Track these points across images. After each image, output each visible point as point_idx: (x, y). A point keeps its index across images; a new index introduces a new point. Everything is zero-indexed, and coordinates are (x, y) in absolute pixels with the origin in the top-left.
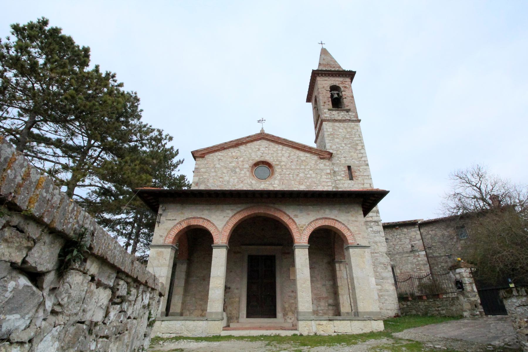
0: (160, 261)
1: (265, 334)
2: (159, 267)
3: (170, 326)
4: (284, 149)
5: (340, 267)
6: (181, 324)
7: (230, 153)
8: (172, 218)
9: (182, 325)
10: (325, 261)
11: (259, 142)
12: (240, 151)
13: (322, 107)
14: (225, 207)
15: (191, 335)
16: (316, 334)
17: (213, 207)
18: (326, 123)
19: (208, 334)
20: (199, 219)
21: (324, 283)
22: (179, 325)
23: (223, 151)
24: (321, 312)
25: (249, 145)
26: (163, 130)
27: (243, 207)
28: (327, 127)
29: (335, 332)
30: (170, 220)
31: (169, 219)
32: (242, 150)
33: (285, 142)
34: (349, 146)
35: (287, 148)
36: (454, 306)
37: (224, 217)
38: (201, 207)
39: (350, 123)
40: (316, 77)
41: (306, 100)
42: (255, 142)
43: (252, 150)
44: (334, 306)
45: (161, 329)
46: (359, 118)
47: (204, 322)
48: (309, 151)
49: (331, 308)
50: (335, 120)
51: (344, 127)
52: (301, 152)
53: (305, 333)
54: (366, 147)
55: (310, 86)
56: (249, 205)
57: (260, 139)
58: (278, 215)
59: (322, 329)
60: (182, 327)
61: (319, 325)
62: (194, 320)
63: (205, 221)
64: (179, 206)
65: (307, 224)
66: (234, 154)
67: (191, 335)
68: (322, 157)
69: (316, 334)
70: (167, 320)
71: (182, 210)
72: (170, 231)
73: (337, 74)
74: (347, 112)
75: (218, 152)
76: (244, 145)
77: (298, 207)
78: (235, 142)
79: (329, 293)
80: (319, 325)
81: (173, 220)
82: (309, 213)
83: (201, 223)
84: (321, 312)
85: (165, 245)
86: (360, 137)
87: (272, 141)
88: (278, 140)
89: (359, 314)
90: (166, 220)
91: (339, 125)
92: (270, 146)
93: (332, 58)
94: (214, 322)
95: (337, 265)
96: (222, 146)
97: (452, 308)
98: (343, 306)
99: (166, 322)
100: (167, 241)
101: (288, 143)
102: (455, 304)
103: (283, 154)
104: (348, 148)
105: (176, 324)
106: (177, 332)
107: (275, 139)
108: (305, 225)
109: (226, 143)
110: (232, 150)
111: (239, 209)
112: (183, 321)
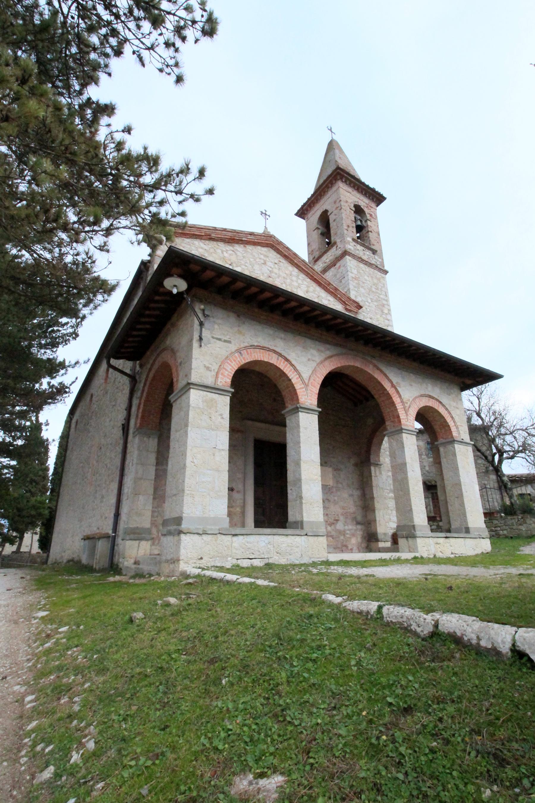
0: (213, 418)
1: (383, 558)
2: (213, 430)
3: (249, 545)
4: (300, 277)
5: (375, 472)
6: (267, 542)
7: (219, 251)
8: (224, 338)
9: (269, 543)
10: (353, 461)
11: (265, 249)
12: (236, 254)
13: (345, 232)
14: (309, 342)
15: (284, 560)
16: (435, 556)
17: (290, 336)
18: (350, 258)
19: (310, 558)
20: (271, 353)
21: (351, 492)
22: (264, 544)
23: (207, 242)
24: (348, 532)
25: (250, 248)
26: (145, 149)
27: (338, 350)
28: (352, 266)
29: (452, 553)
30: (220, 339)
31: (219, 337)
32: (238, 253)
33: (304, 266)
34: (376, 303)
35: (304, 276)
36: (525, 525)
37: (309, 360)
38: (271, 332)
39: (376, 272)
40: (336, 180)
41: (296, 211)
42: (259, 247)
43: (255, 260)
44: (362, 524)
45: (234, 551)
46: (386, 268)
47: (303, 537)
48: (332, 293)
49: (359, 527)
50: (360, 258)
51: (370, 274)
52: (323, 291)
53: (425, 555)
54: (393, 312)
55: (373, 190)
56: (344, 351)
57: (267, 245)
58: (377, 376)
59: (440, 550)
60: (269, 546)
61: (437, 543)
62: (287, 535)
63: (280, 358)
64: (232, 318)
65: (411, 400)
66: (225, 254)
67: (284, 560)
68: (348, 307)
69: (435, 556)
70: (243, 535)
71: (239, 326)
72: (223, 362)
73: (364, 189)
74: (374, 254)
75: (198, 240)
76: (242, 246)
77: (399, 371)
78: (230, 234)
79: (357, 506)
80: (437, 543)
81: (225, 341)
82: (413, 384)
83: (273, 359)
84: (348, 532)
85: (216, 386)
86: (386, 295)
87: (286, 257)
88: (295, 258)
89: (471, 530)
90: (213, 337)
91: (364, 269)
92: (281, 264)
93: (348, 161)
94: (316, 538)
95: (372, 468)
96: (208, 232)
97: (520, 527)
98: (380, 525)
99: (241, 537)
100: (219, 380)
101: (307, 268)
102: (526, 523)
103: (299, 284)
104: (374, 306)
105: (258, 542)
106: (263, 556)
107: (289, 254)
108: (409, 400)
109: (215, 229)
110: (221, 245)
111: (328, 353)
112: (270, 536)
